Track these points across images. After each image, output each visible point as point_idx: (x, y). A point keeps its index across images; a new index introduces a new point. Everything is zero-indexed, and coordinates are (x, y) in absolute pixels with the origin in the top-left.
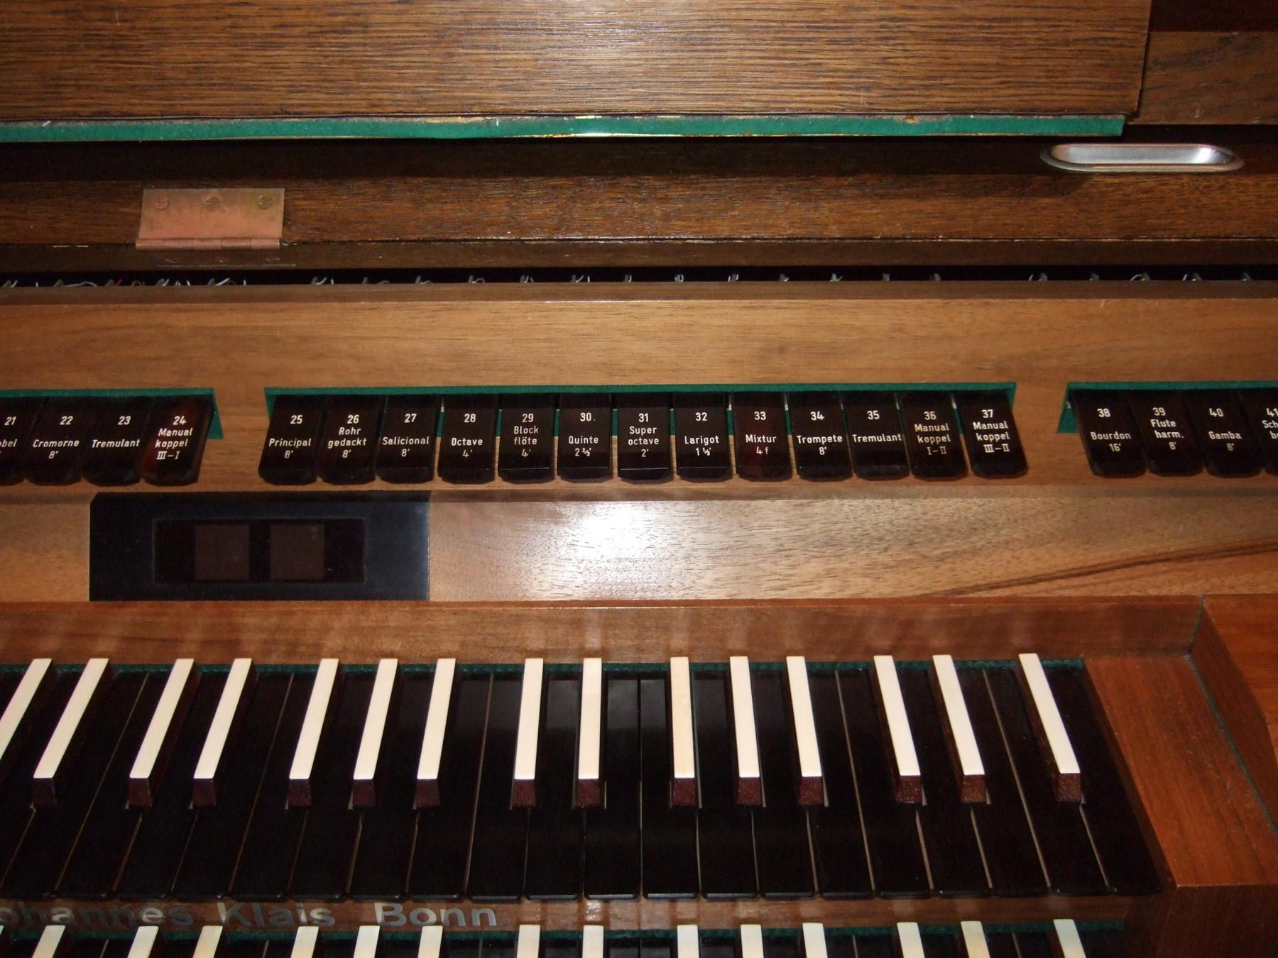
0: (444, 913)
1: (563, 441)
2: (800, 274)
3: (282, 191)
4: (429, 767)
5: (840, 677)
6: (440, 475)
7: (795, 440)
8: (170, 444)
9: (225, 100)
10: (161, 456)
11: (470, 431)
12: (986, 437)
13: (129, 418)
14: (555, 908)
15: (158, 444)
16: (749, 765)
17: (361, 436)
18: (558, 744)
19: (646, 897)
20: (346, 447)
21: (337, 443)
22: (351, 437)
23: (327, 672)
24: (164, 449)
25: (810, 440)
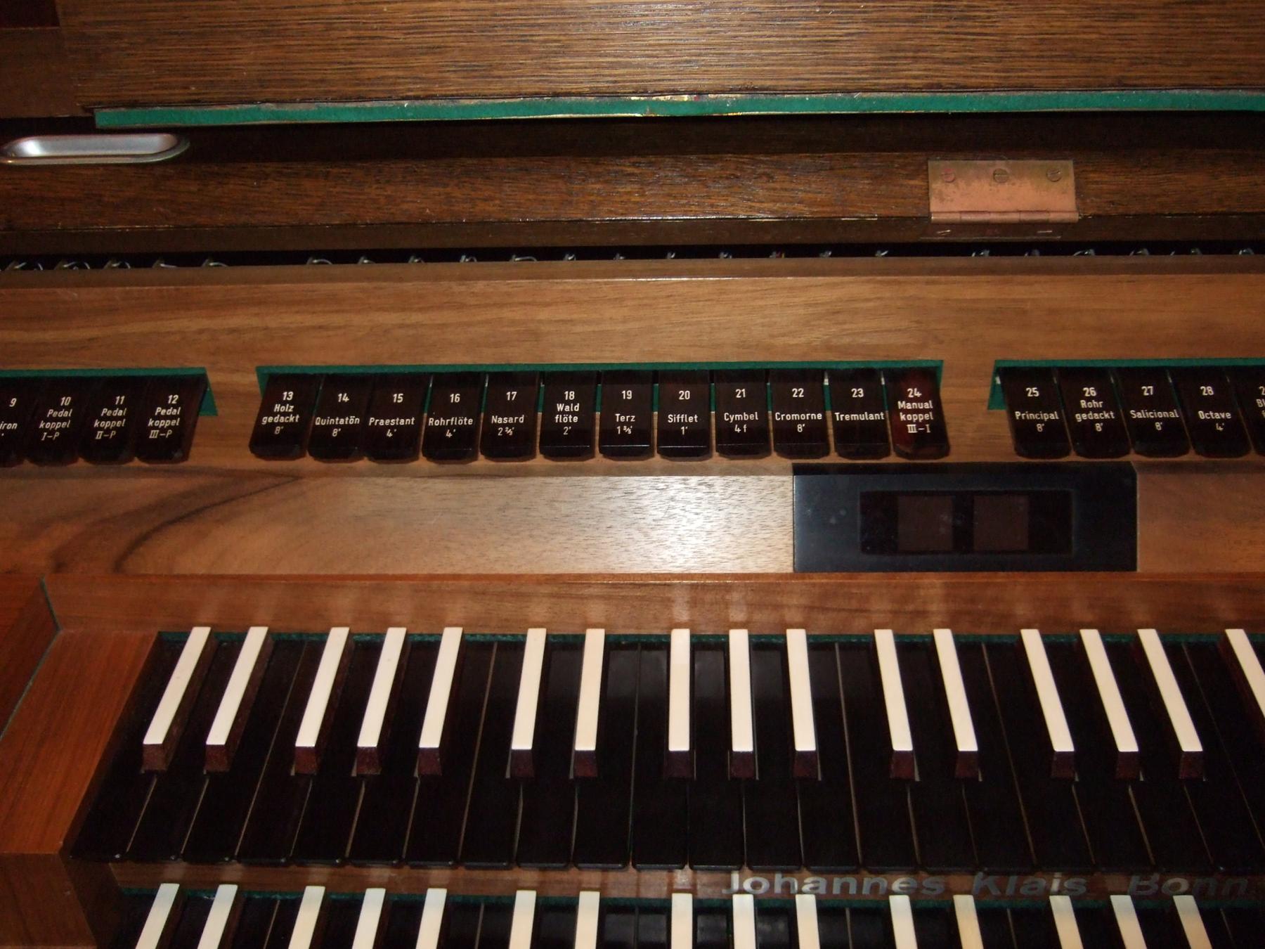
0: (822, 882)
1: (663, 418)
2: (842, 250)
3: (1070, 163)
4: (431, 736)
5: (840, 648)
6: (541, 452)
7: (834, 417)
8: (162, 423)
9: (1063, 73)
10: (154, 434)
11: (686, 408)
12: (909, 417)
13: (291, 394)
14: (612, 876)
15: (151, 423)
16: (743, 739)
17: (1106, 408)
18: (710, 713)
19: (634, 866)
20: (279, 424)
21: (270, 419)
22: (285, 414)
23: (337, 640)
24: (157, 428)
25: (788, 417)
